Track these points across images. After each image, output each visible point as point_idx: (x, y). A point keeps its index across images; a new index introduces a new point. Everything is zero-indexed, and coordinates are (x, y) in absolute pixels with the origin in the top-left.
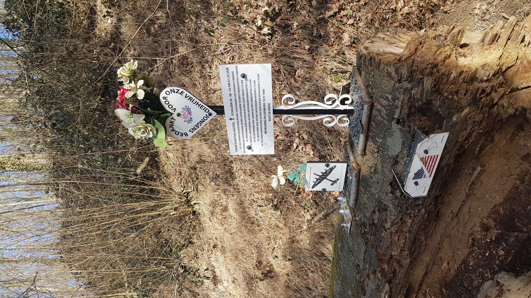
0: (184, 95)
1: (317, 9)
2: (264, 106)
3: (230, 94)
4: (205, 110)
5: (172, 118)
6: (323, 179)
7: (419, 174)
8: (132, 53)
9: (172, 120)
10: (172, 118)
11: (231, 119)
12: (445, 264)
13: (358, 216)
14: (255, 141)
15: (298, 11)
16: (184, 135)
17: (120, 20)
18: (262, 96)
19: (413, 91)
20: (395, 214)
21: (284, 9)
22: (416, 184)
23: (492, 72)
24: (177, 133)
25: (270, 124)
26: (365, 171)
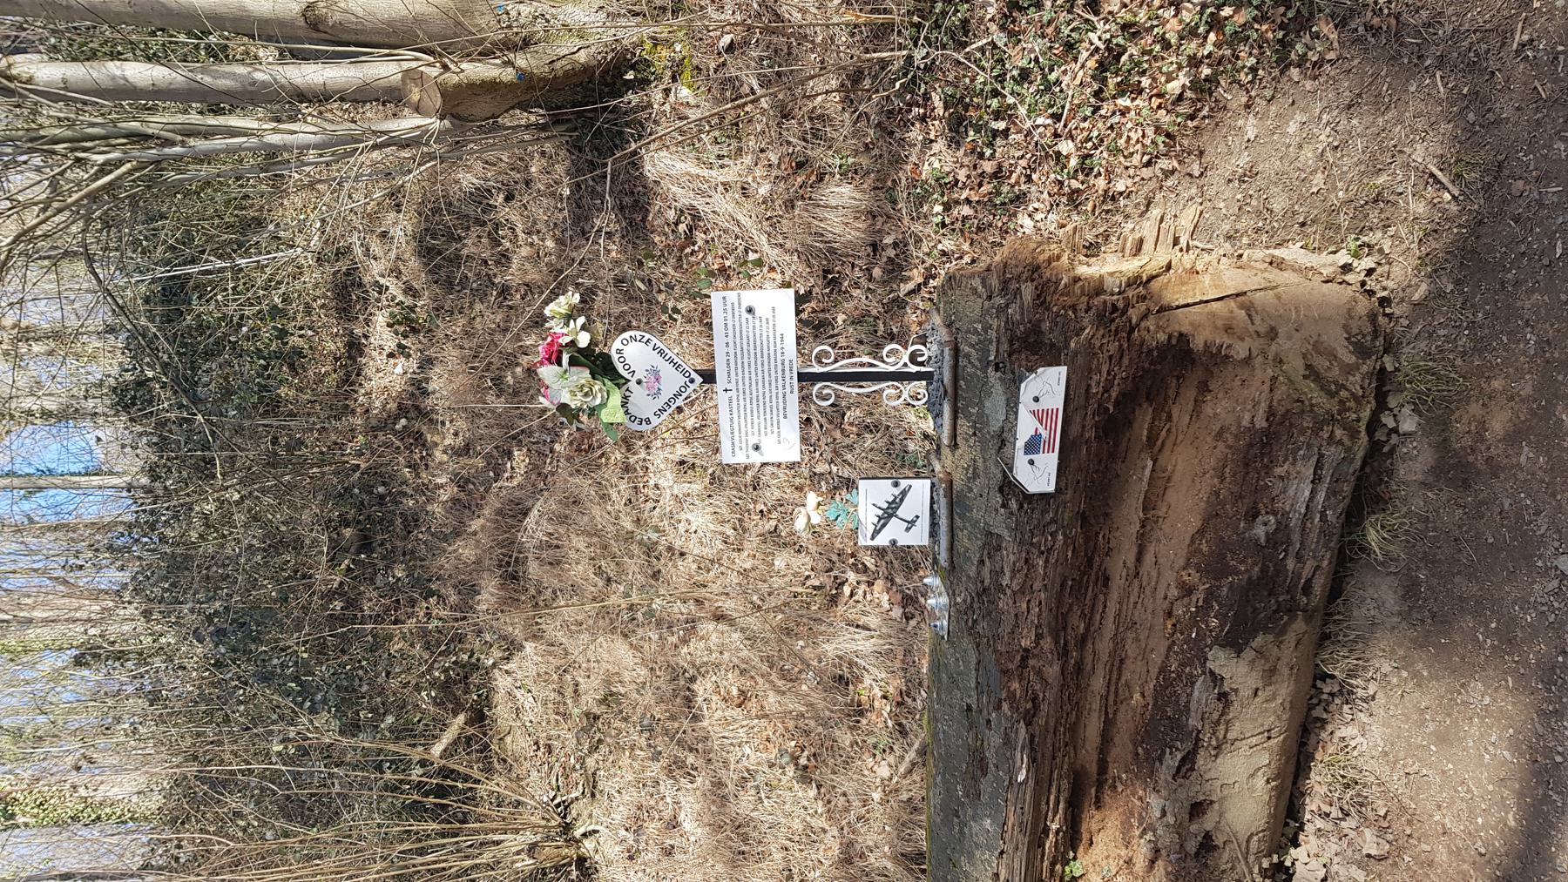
1: (884, 283)
4: (684, 373)
6: (890, 516)
7: (1033, 446)
8: (447, 442)
12: (1137, 696)
15: (846, 292)
17: (427, 363)
21: (816, 290)
22: (1031, 462)
23: (1124, 280)
25: (794, 399)
26: (959, 479)
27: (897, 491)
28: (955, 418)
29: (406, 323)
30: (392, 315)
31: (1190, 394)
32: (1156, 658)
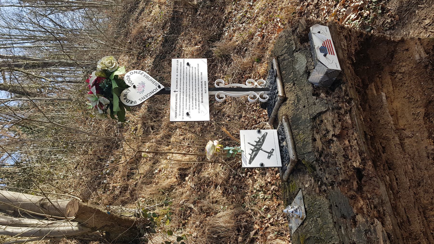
0: (143, 75)
2: (202, 82)
6: (258, 149)
24: (128, 101)
27: (260, 136)
31: (388, 79)
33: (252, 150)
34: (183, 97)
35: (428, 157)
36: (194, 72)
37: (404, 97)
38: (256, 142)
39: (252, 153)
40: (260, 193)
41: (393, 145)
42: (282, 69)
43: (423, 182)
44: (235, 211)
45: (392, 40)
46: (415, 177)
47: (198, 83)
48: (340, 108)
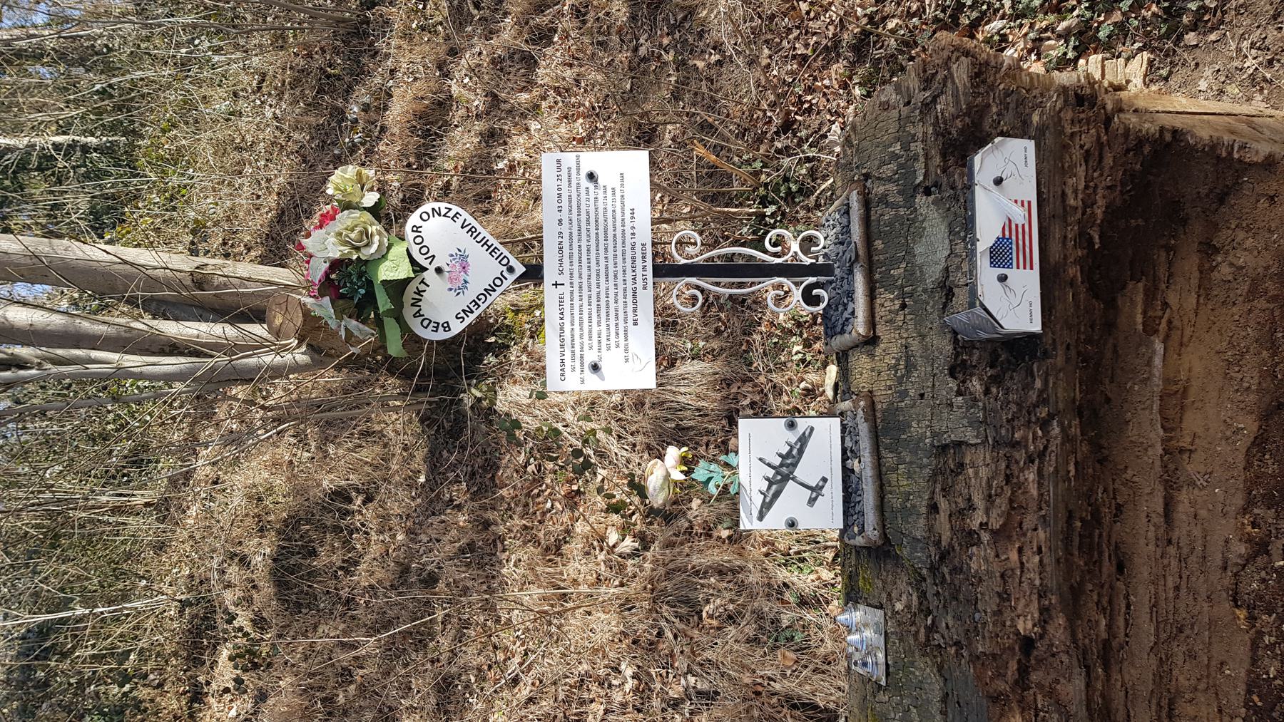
0: (460, 221)
2: (633, 249)
3: (560, 221)
4: (501, 259)
5: (422, 281)
6: (786, 478)
7: (1000, 255)
9: (422, 287)
10: (422, 281)
11: (556, 285)
13: (899, 600)
14: (609, 349)
16: (441, 328)
18: (628, 224)
19: (938, 107)
20: (988, 461)
24: (426, 323)
26: (883, 396)
27: (793, 437)
28: (871, 296)
29: (249, 660)
30: (236, 647)
31: (1190, 264)
32: (1237, 671)
33: (768, 479)
34: (581, 306)
35: (1225, 569)
36: (610, 209)
37: (1218, 353)
38: (780, 455)
39: (769, 488)
40: (793, 339)
41: (1144, 514)
42: (874, 228)
43: (1192, 628)
44: (727, 371)
45: (1236, 156)
46: (1176, 610)
47: (624, 252)
48: (1015, 445)
